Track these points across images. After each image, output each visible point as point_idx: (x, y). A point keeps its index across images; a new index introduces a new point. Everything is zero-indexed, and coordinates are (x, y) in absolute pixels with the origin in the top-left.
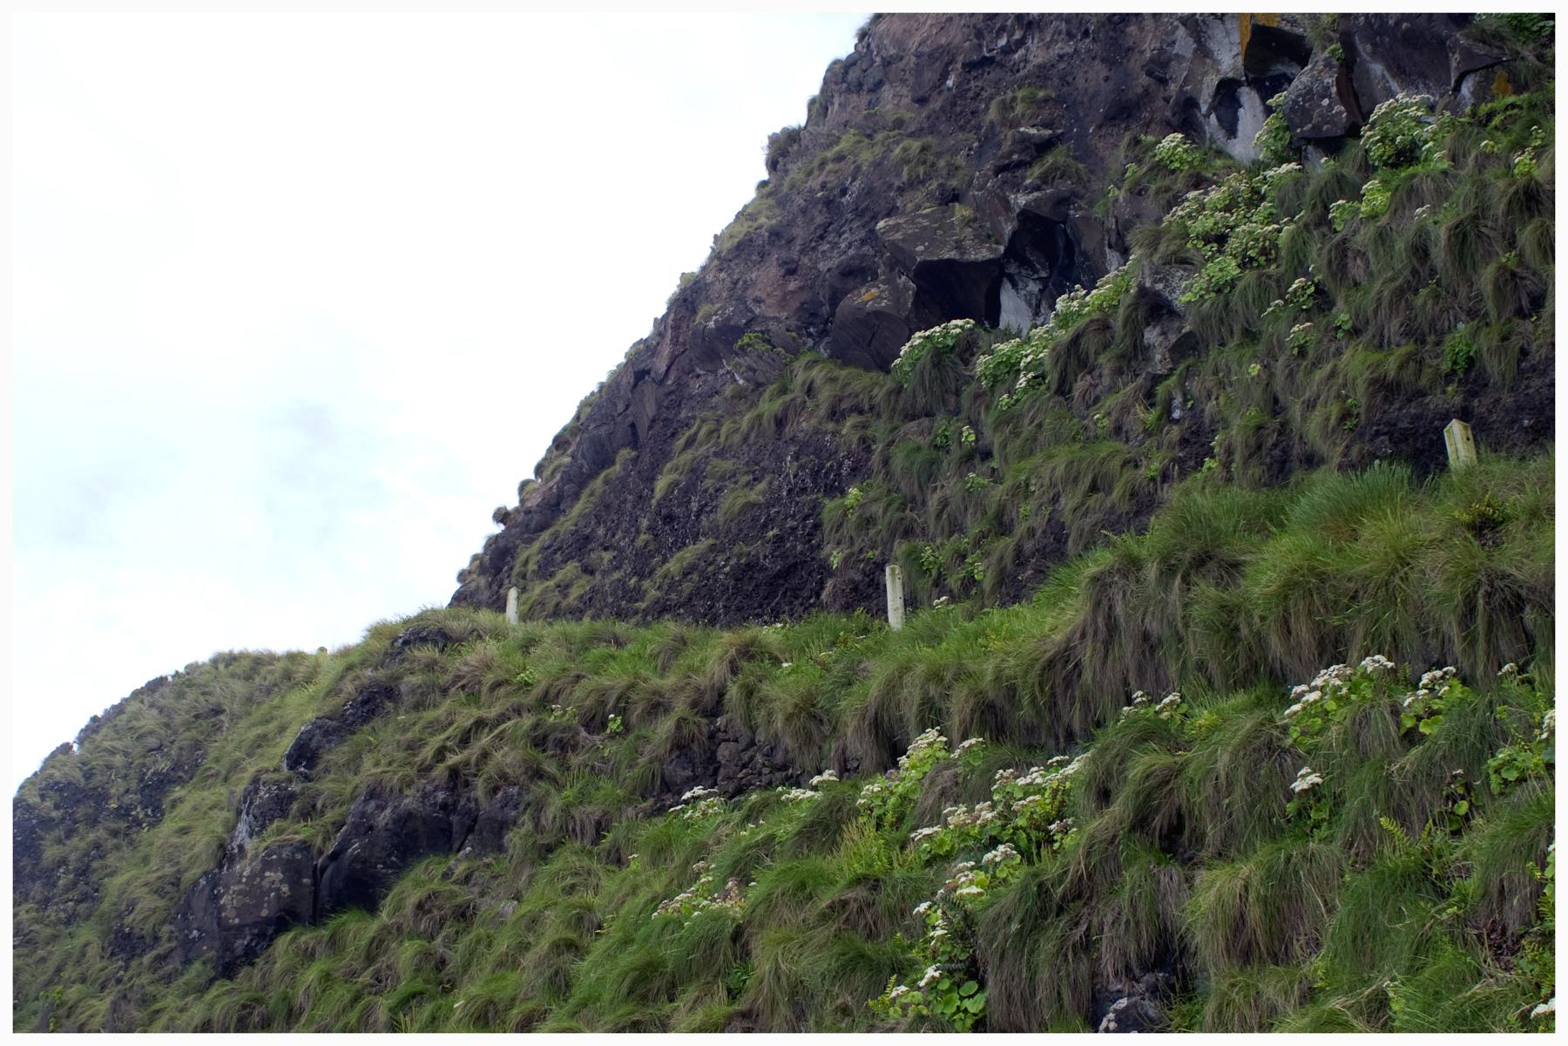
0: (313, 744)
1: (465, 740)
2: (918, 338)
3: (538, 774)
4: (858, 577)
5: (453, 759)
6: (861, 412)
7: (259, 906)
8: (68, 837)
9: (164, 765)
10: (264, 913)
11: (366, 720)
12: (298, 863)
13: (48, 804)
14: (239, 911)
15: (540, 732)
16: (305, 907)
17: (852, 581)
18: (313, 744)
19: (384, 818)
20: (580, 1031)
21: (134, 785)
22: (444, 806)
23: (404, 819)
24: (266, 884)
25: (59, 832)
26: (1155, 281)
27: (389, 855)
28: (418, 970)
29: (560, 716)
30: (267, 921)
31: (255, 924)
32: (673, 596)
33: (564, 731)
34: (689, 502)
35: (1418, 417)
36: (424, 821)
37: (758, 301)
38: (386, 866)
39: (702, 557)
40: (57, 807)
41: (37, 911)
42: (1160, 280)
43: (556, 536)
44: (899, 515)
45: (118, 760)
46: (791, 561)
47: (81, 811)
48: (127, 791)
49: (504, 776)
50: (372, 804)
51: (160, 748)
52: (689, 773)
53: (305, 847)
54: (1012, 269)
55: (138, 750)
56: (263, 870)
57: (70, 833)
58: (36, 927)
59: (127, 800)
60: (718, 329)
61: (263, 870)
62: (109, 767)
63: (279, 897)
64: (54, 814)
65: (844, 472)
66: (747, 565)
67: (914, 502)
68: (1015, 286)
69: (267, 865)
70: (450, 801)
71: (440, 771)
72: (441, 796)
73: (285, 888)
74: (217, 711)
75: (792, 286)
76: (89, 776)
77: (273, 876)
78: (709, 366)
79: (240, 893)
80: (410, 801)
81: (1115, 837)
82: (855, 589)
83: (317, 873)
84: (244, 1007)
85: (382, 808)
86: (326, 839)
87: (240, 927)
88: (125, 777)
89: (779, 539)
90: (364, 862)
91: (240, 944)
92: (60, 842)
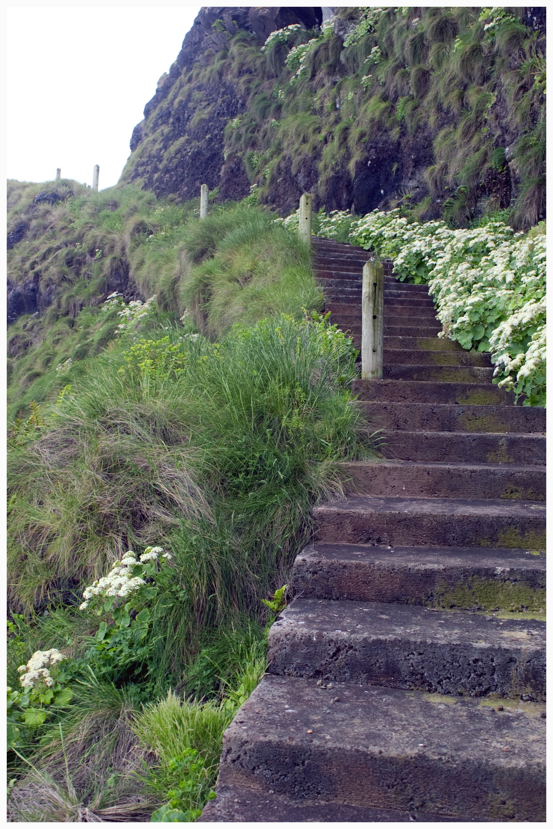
1: (44, 257)
3: (64, 279)
4: (233, 166)
5: (38, 268)
6: (251, 73)
17: (231, 168)
26: (340, 30)
27: (13, 312)
29: (80, 249)
32: (171, 165)
34: (184, 113)
35: (386, 142)
36: (25, 296)
39: (183, 145)
43: (161, 109)
46: (213, 152)
49: (50, 280)
52: (119, 282)
66: (197, 152)
67: (256, 129)
70: (36, 287)
71: (31, 274)
72: (31, 285)
78: (210, 31)
82: (232, 171)
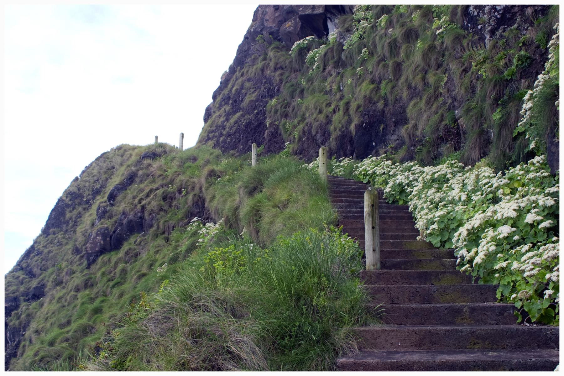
0: (115, 194)
2: (297, 43)
3: (161, 209)
4: (273, 131)
5: (143, 202)
6: (283, 69)
7: (95, 247)
8: (73, 210)
9: (98, 186)
10: (97, 249)
11: (130, 184)
12: (105, 234)
13: (68, 199)
14: (91, 248)
15: (165, 194)
16: (108, 247)
17: (271, 132)
18: (115, 194)
19: (125, 221)
20: (6, 350)
21: (90, 193)
22: (141, 218)
23: (130, 222)
24: (97, 240)
25: (71, 209)
28: (121, 275)
29: (171, 189)
30: (98, 252)
31: (95, 253)
33: (172, 194)
37: (267, 20)
38: (126, 236)
39: (239, 118)
40: (70, 200)
41: (64, 234)
42: (342, 38)
43: (224, 94)
44: (284, 110)
45: (87, 184)
47: (77, 201)
48: (89, 195)
49: (152, 210)
50: (123, 216)
51: (98, 180)
53: (107, 229)
54: (329, 15)
55: (92, 181)
56: (96, 236)
57: (74, 208)
58: (63, 240)
59: (88, 198)
60: (254, 32)
61: (96, 236)
62: (85, 186)
63: (100, 245)
64: (70, 203)
65: (275, 91)
67: (287, 105)
68: (331, 20)
69: (97, 235)
71: (139, 207)
72: (139, 214)
73: (102, 242)
74: (114, 168)
75: (277, 14)
76: (79, 190)
77: (99, 238)
79: (91, 243)
80: (131, 217)
81: (109, 308)
82: (272, 134)
83: (111, 237)
84: (87, 280)
85: (125, 217)
86: (112, 227)
87: (91, 253)
88: (88, 190)
89: (257, 114)
90: (120, 234)
91: (91, 258)
92: (71, 212)
